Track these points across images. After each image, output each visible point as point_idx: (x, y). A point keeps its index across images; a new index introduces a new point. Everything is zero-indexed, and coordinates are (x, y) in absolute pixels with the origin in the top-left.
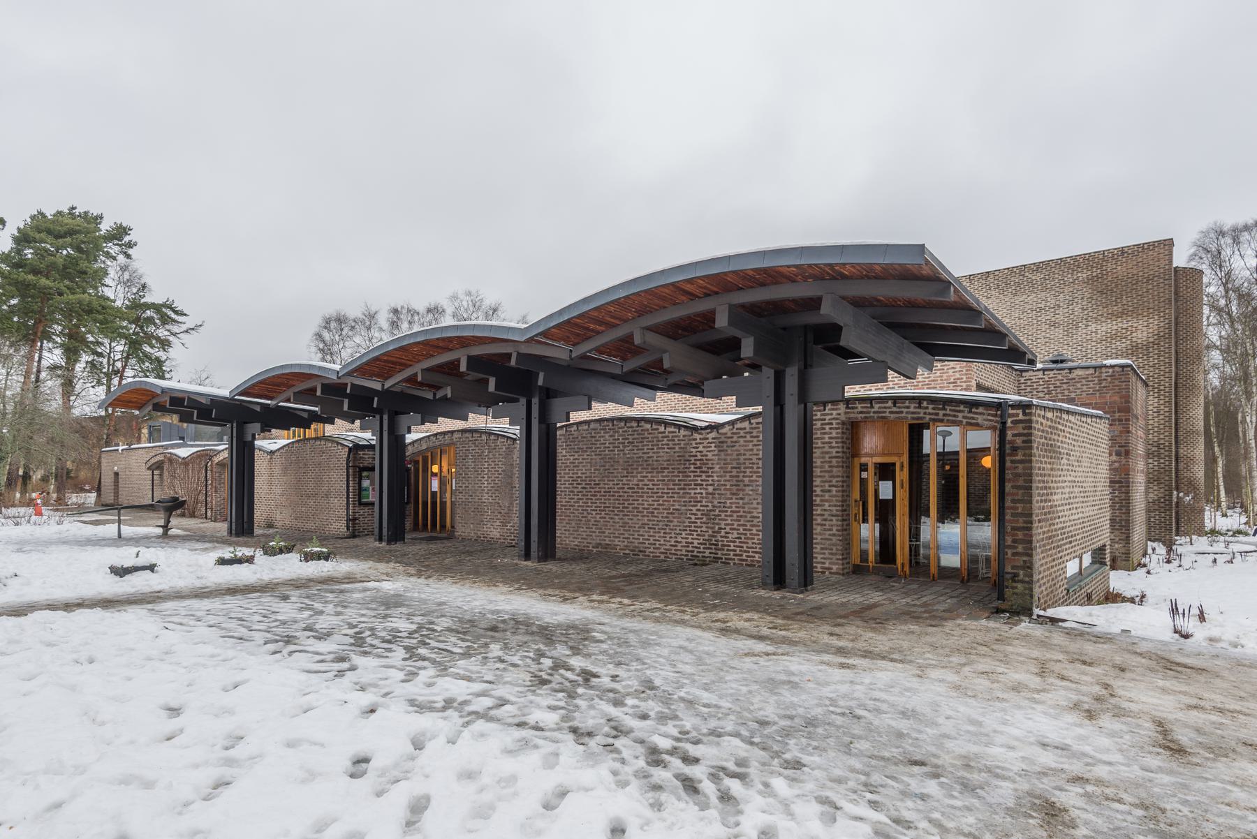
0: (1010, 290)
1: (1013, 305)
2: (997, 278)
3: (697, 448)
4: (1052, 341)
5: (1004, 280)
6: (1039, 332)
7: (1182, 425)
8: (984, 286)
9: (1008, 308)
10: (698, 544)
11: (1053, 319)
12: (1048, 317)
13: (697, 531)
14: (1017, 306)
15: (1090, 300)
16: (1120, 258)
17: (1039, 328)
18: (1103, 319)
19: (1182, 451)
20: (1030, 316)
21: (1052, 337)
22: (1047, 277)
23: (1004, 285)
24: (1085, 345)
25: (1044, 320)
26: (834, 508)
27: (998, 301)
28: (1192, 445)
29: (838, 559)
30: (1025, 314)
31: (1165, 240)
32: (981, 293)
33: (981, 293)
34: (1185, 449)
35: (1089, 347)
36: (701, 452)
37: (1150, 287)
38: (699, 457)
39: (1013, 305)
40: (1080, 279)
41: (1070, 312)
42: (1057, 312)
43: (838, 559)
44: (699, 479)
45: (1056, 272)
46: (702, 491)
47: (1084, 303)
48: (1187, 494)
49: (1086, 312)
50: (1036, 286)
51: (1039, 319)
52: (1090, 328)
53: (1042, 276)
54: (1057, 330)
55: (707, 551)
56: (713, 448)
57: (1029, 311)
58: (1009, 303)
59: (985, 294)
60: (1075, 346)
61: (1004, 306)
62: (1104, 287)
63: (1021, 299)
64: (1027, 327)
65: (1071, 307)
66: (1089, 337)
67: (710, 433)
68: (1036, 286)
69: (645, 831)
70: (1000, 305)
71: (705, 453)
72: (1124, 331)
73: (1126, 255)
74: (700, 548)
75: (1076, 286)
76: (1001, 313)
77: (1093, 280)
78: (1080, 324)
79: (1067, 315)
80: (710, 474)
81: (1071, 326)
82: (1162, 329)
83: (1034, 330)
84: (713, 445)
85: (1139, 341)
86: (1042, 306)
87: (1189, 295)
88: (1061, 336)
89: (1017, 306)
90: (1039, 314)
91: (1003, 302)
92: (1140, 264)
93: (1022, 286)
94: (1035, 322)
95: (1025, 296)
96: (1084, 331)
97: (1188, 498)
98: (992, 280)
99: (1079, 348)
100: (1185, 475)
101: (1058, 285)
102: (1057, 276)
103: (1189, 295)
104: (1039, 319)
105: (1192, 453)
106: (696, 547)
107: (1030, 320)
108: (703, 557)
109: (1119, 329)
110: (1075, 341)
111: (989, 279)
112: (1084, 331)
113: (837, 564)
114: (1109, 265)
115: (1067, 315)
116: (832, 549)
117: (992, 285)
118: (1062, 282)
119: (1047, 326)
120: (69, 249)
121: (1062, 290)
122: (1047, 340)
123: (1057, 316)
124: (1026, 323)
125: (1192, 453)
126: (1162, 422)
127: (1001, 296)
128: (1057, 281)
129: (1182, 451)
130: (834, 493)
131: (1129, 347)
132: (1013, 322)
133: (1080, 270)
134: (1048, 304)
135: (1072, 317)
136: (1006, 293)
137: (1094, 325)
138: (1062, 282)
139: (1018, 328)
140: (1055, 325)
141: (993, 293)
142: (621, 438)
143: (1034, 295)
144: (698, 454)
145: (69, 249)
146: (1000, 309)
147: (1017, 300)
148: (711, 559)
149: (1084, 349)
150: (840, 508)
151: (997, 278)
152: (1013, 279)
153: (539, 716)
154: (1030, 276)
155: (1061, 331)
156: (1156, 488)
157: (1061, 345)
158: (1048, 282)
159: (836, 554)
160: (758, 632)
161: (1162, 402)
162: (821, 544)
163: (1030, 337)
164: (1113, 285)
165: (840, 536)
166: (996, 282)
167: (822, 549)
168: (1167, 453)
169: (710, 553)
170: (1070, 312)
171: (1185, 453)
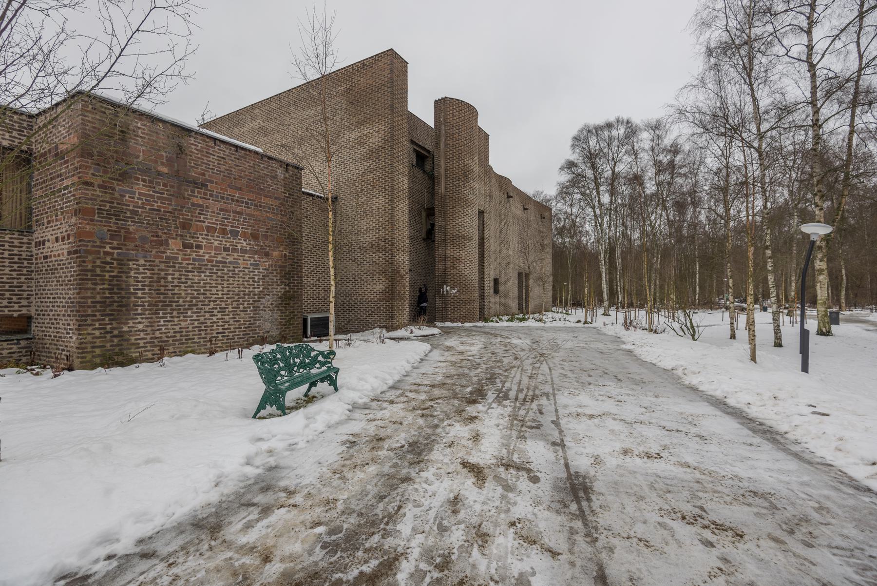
7: (449, 230)
18: (353, 128)
19: (449, 252)
28: (458, 247)
31: (388, 51)
34: (452, 250)
37: (380, 95)
48: (452, 288)
69: (532, 568)
72: (365, 137)
77: (348, 91)
82: (386, 134)
85: (374, 146)
87: (455, 122)
95: (310, 110)
97: (454, 291)
100: (452, 272)
103: (455, 122)
105: (458, 254)
125: (458, 254)
126: (387, 219)
129: (449, 252)
131: (368, 152)
153: (490, 525)
156: (384, 279)
160: (276, 500)
161: (387, 200)
168: (390, 247)
171: (452, 254)
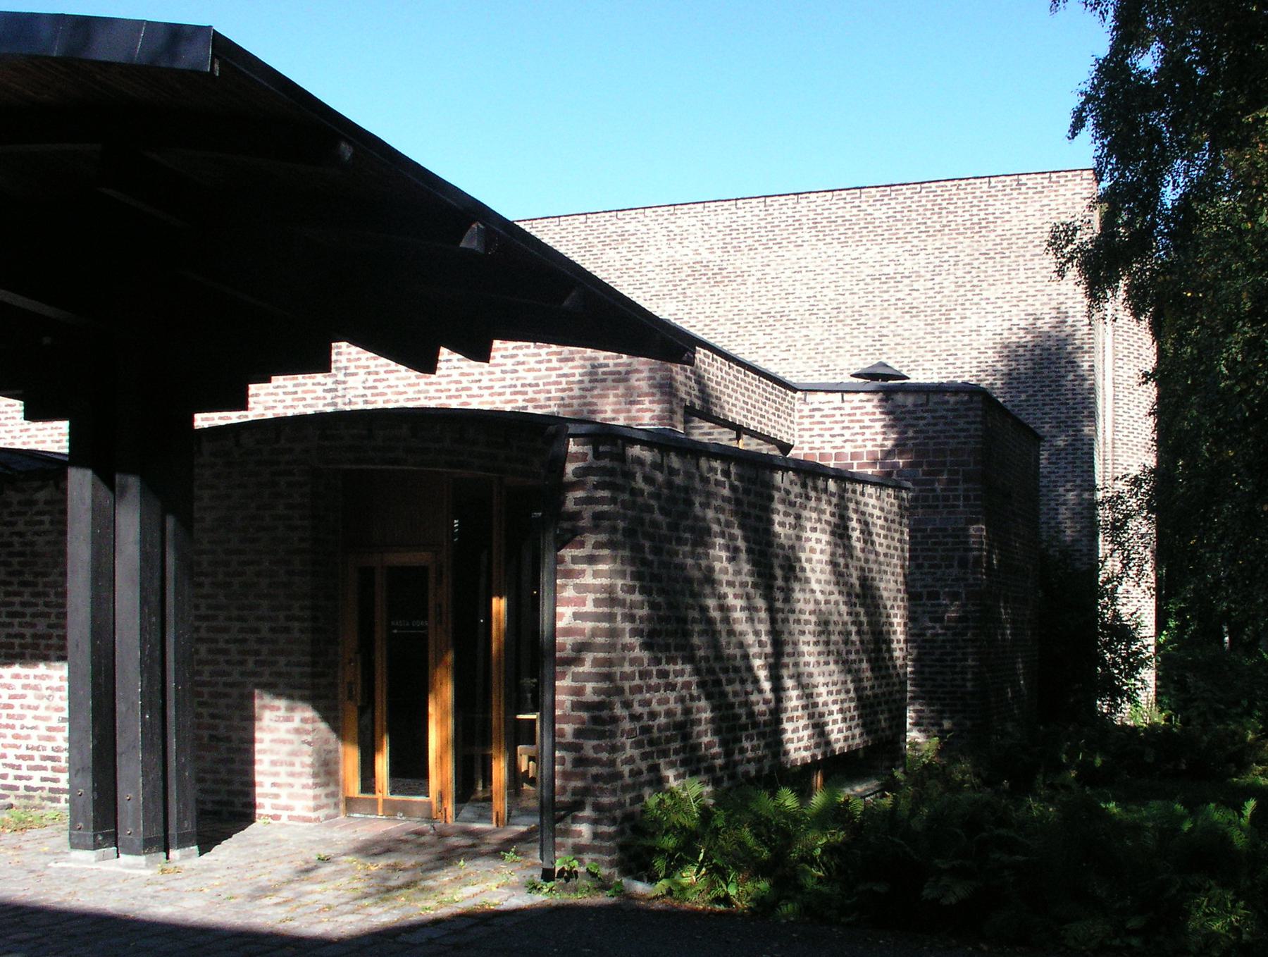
0: (836, 234)
1: (841, 264)
2: (813, 206)
3: (13, 524)
4: (907, 343)
5: (826, 214)
6: (885, 323)
8: (790, 221)
9: (833, 269)
10: (18, 757)
11: (909, 299)
12: (900, 295)
13: (13, 727)
14: (847, 268)
15: (968, 268)
16: (1015, 193)
17: (886, 314)
20: (870, 289)
21: (907, 334)
22: (899, 216)
23: (825, 223)
24: (960, 354)
25: (893, 301)
26: (297, 670)
27: (815, 253)
29: (304, 786)
30: (862, 285)
32: (785, 234)
33: (785, 234)
35: (967, 360)
36: (20, 534)
38: (17, 548)
39: (841, 264)
40: (953, 226)
41: (937, 288)
42: (916, 286)
43: (304, 786)
44: (17, 599)
45: (914, 207)
46: (23, 630)
47: (959, 273)
49: (962, 291)
50: (879, 231)
51: (886, 296)
52: (967, 322)
53: (891, 213)
54: (915, 321)
55: (37, 775)
56: (47, 526)
57: (868, 280)
58: (833, 261)
59: (793, 238)
60: (944, 356)
61: (825, 265)
62: (990, 245)
63: (855, 255)
64: (864, 311)
65: (938, 279)
66: (966, 340)
67: (40, 488)
68: (879, 231)
70: (818, 261)
71: (29, 537)
73: (1024, 189)
74: (19, 767)
75: (946, 239)
76: (819, 278)
78: (953, 314)
79: (931, 293)
80: (40, 589)
81: (937, 316)
83: (877, 319)
84: (46, 518)
86: (890, 270)
88: (921, 334)
89: (847, 268)
90: (885, 287)
91: (824, 256)
92: (1046, 209)
93: (856, 228)
94: (878, 301)
95: (862, 249)
96: (959, 327)
98: (805, 211)
99: (951, 359)
101: (916, 233)
102: (914, 215)
104: (886, 296)
106: (12, 766)
107: (870, 296)
108: (27, 788)
109: (1015, 328)
110: (944, 346)
111: (799, 207)
112: (959, 327)
113: (304, 797)
114: (998, 203)
115: (931, 293)
116: (292, 764)
117: (804, 220)
118: (923, 228)
119: (899, 313)
120: (1246, 240)
121: (922, 245)
122: (898, 340)
123: (915, 294)
124: (863, 302)
127: (820, 244)
128: (914, 225)
130: (297, 634)
132: (841, 299)
133: (952, 208)
134: (900, 269)
135: (939, 297)
136: (828, 239)
137: (975, 318)
138: (923, 228)
139: (849, 312)
140: (911, 311)
141: (807, 237)
142: (926, 564)
143: (877, 249)
144: (16, 539)
145: (1246, 240)
146: (818, 271)
147: (852, 251)
148: (46, 794)
149: (959, 364)
150: (308, 670)
151: (813, 206)
152: (840, 213)
154: (870, 210)
155: (922, 324)
157: (921, 351)
158: (899, 225)
159: (300, 774)
162: (272, 751)
163: (870, 332)
164: (1005, 244)
165: (308, 732)
166: (811, 215)
167: (273, 763)
169: (44, 779)
170: (937, 288)
